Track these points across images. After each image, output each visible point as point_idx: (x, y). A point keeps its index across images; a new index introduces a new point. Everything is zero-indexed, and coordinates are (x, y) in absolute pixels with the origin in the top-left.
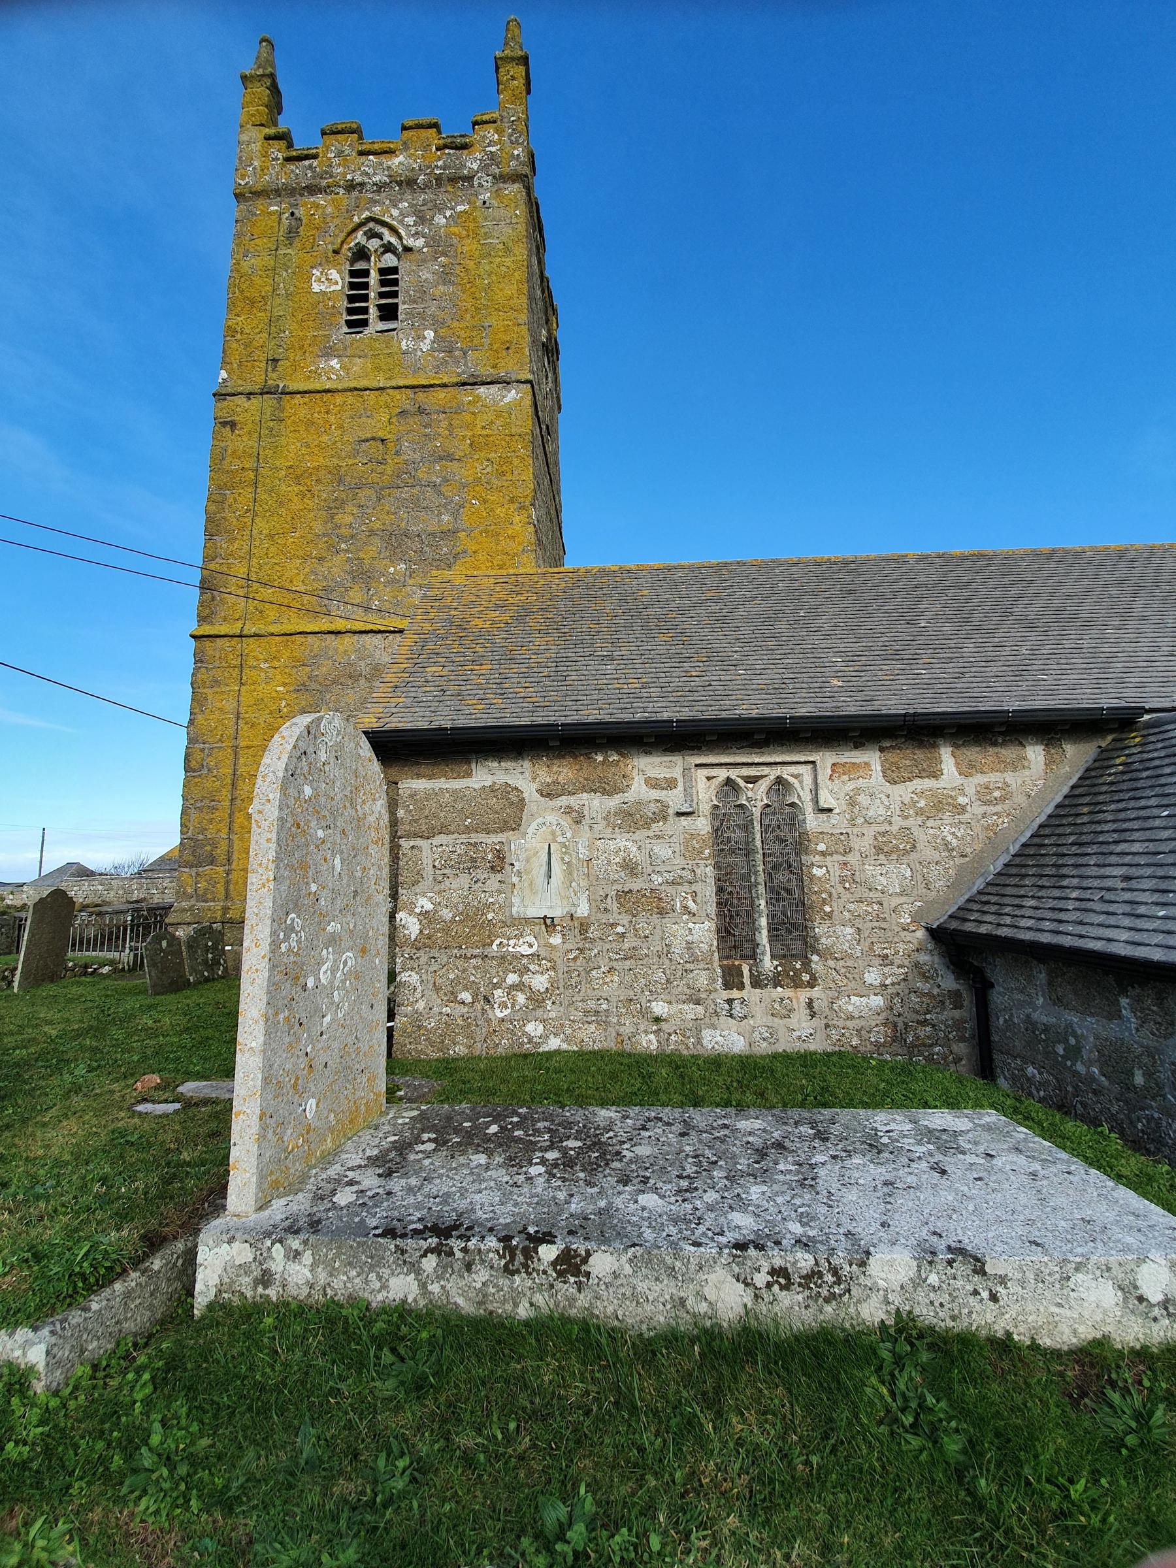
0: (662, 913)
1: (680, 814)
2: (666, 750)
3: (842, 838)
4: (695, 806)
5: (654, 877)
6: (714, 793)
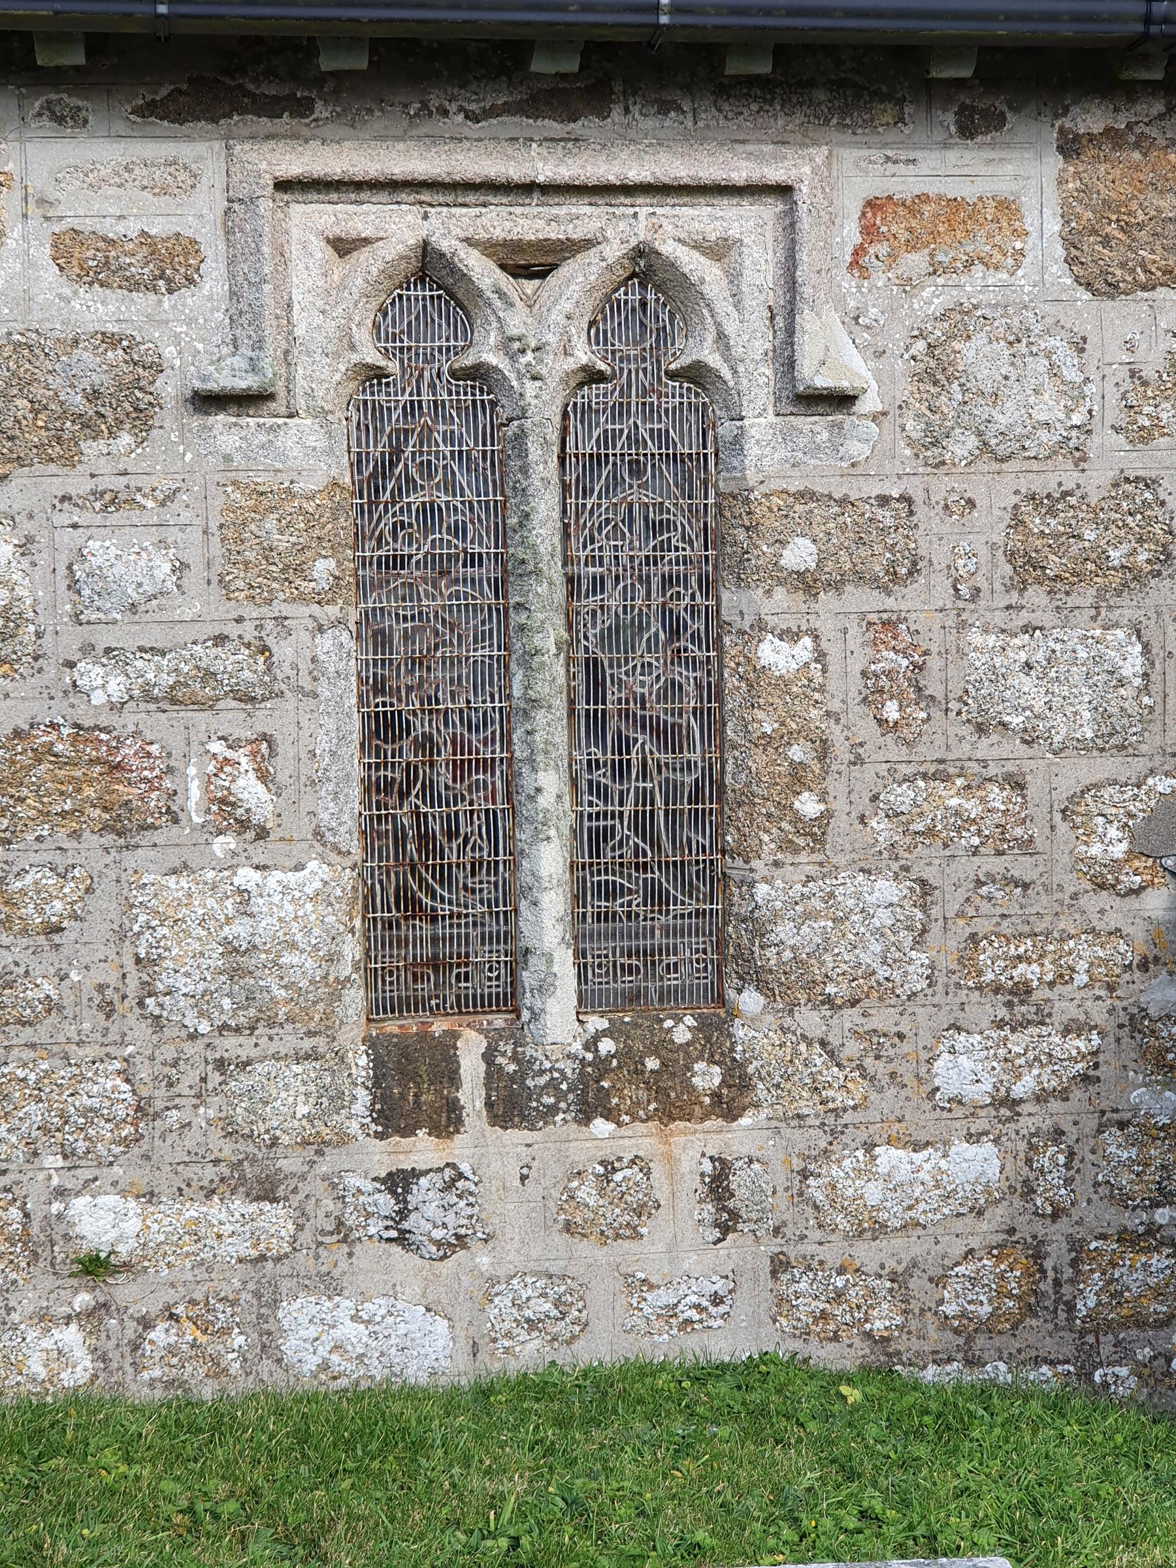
0: (123, 825)
1: (209, 402)
2: (149, 110)
3: (886, 517)
4: (269, 366)
5: (90, 673)
6: (366, 314)
